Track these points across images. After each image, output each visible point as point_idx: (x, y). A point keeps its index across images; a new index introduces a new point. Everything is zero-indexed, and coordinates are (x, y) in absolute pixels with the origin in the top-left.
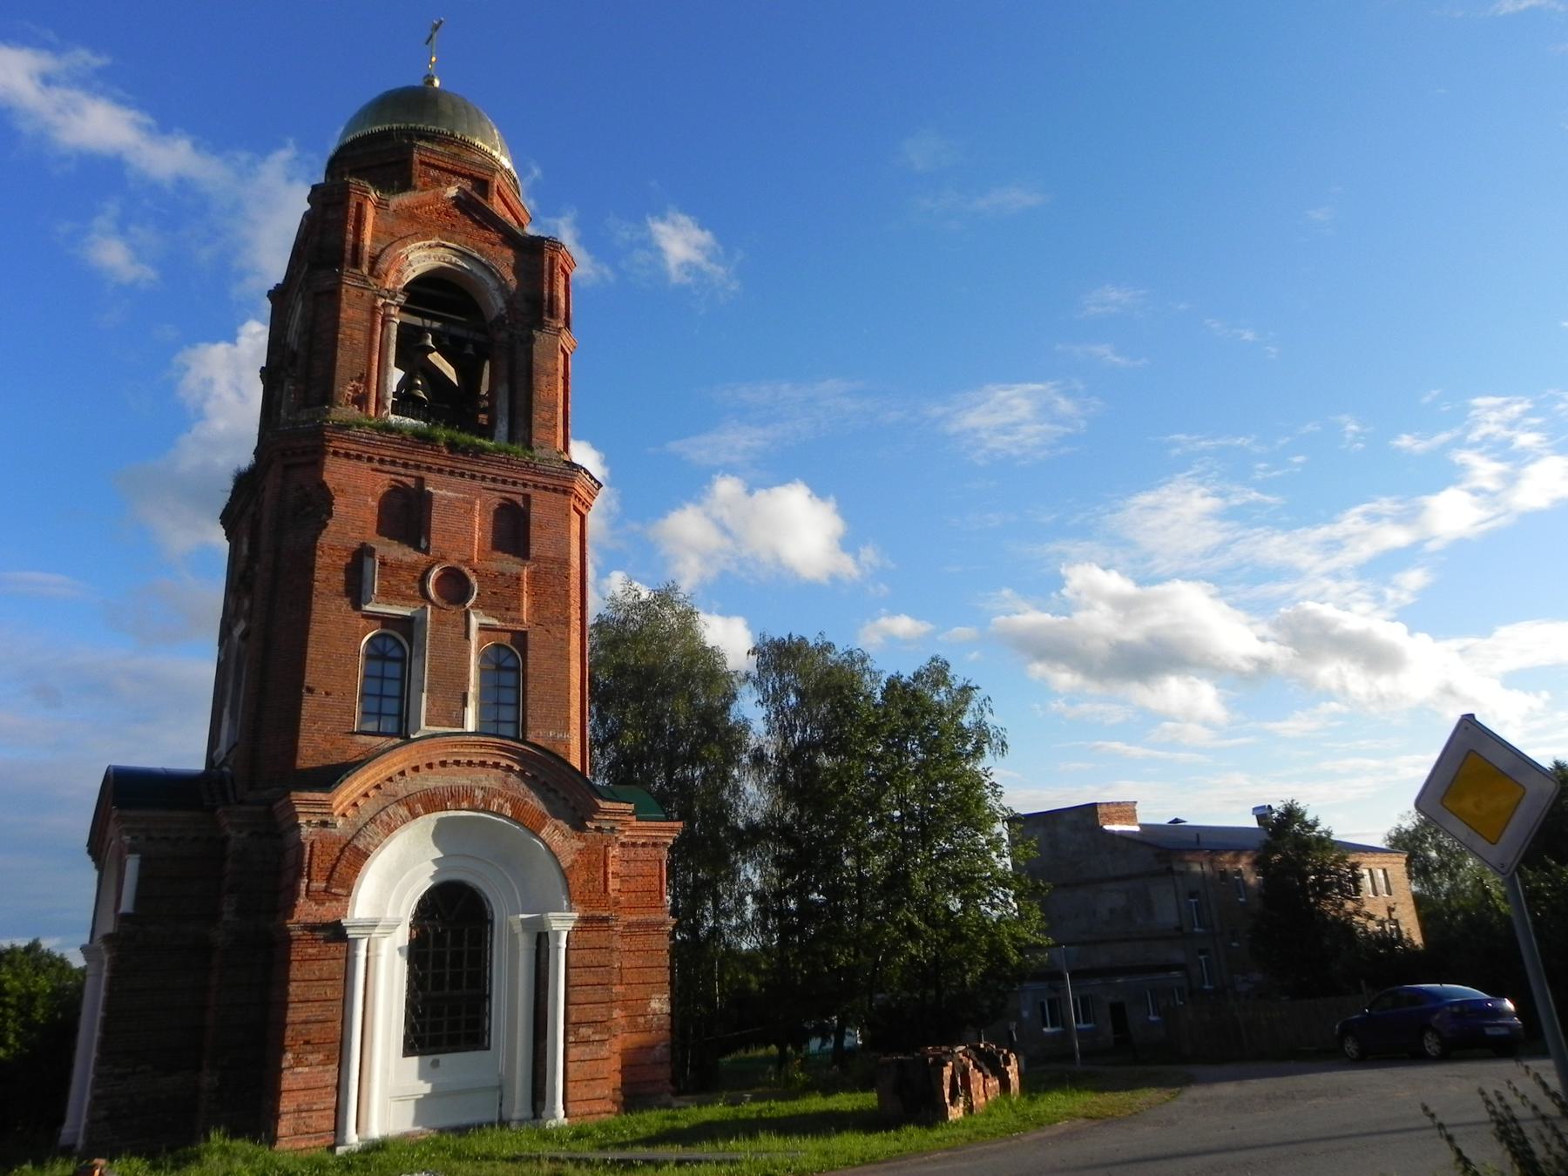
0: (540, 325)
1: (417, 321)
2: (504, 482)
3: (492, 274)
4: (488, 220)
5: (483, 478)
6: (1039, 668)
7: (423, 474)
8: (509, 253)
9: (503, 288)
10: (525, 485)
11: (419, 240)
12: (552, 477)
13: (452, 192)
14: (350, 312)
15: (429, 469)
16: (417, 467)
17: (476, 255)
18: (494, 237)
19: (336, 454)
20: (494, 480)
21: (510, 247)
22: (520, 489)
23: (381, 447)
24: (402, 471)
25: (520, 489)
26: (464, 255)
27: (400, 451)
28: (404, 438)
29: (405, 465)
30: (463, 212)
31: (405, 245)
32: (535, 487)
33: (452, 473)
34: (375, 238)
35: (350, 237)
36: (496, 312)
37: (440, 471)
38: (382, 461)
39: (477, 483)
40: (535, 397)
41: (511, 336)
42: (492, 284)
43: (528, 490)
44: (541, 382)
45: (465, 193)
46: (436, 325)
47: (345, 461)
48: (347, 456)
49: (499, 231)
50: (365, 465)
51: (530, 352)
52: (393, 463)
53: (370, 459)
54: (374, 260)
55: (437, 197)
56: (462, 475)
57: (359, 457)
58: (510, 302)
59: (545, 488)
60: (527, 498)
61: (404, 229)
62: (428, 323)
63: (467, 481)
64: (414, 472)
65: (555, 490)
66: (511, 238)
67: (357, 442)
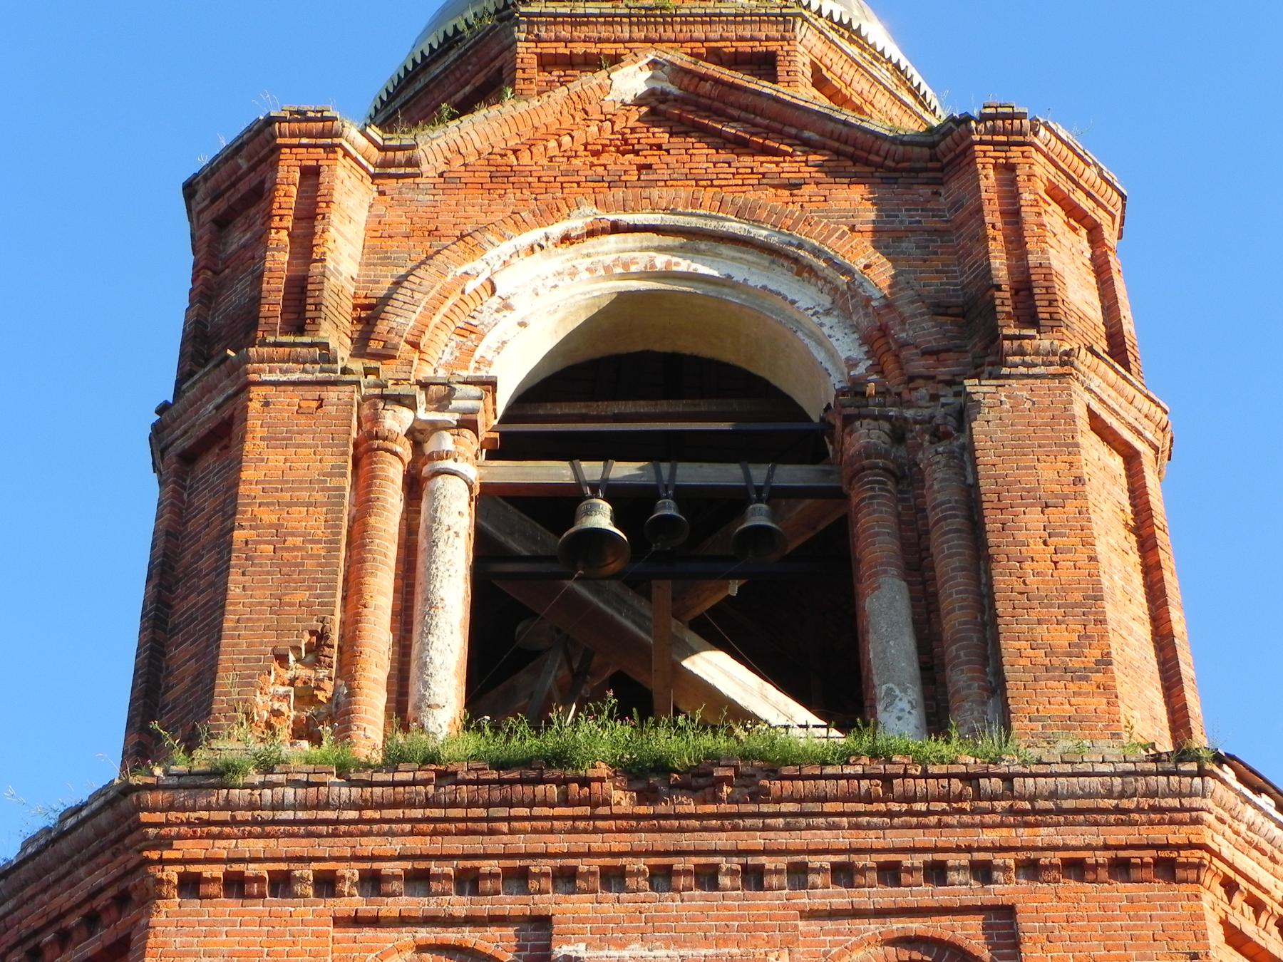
0: (990, 358)
1: (556, 472)
2: (890, 873)
3: (802, 269)
4: (772, 128)
5: (799, 875)
6: (775, 240)
7: (548, 902)
8: (855, 201)
9: (846, 296)
10: (983, 872)
11: (521, 226)
12: (1091, 816)
13: (631, 80)
14: (276, 459)
15: (566, 878)
16: (518, 878)
17: (735, 227)
18: (795, 166)
19: (191, 886)
20: (844, 874)
21: (856, 179)
22: (963, 889)
23: (362, 827)
24: (459, 905)
25: (963, 889)
26: (693, 238)
27: (437, 828)
28: (446, 776)
29: (469, 882)
30: (680, 128)
31: (476, 250)
32: (1031, 869)
33: (662, 877)
34: (375, 252)
35: (279, 259)
36: (836, 380)
37: (613, 878)
38: (373, 882)
39: (766, 901)
40: (1002, 582)
41: (899, 434)
42: (805, 297)
43: (1003, 890)
44: (1023, 536)
45: (679, 72)
46: (624, 470)
47: (230, 907)
48: (236, 885)
49: (810, 146)
50: (308, 912)
51: (965, 458)
52: (419, 880)
53: (327, 884)
54: (370, 314)
55: (582, 107)
56: (707, 878)
57: (282, 884)
58: (878, 340)
59: (1076, 868)
60: (1002, 920)
61: (473, 209)
62: (592, 470)
63: (733, 899)
64: (510, 904)
65: (1121, 868)
66: (852, 153)
67: (263, 828)
